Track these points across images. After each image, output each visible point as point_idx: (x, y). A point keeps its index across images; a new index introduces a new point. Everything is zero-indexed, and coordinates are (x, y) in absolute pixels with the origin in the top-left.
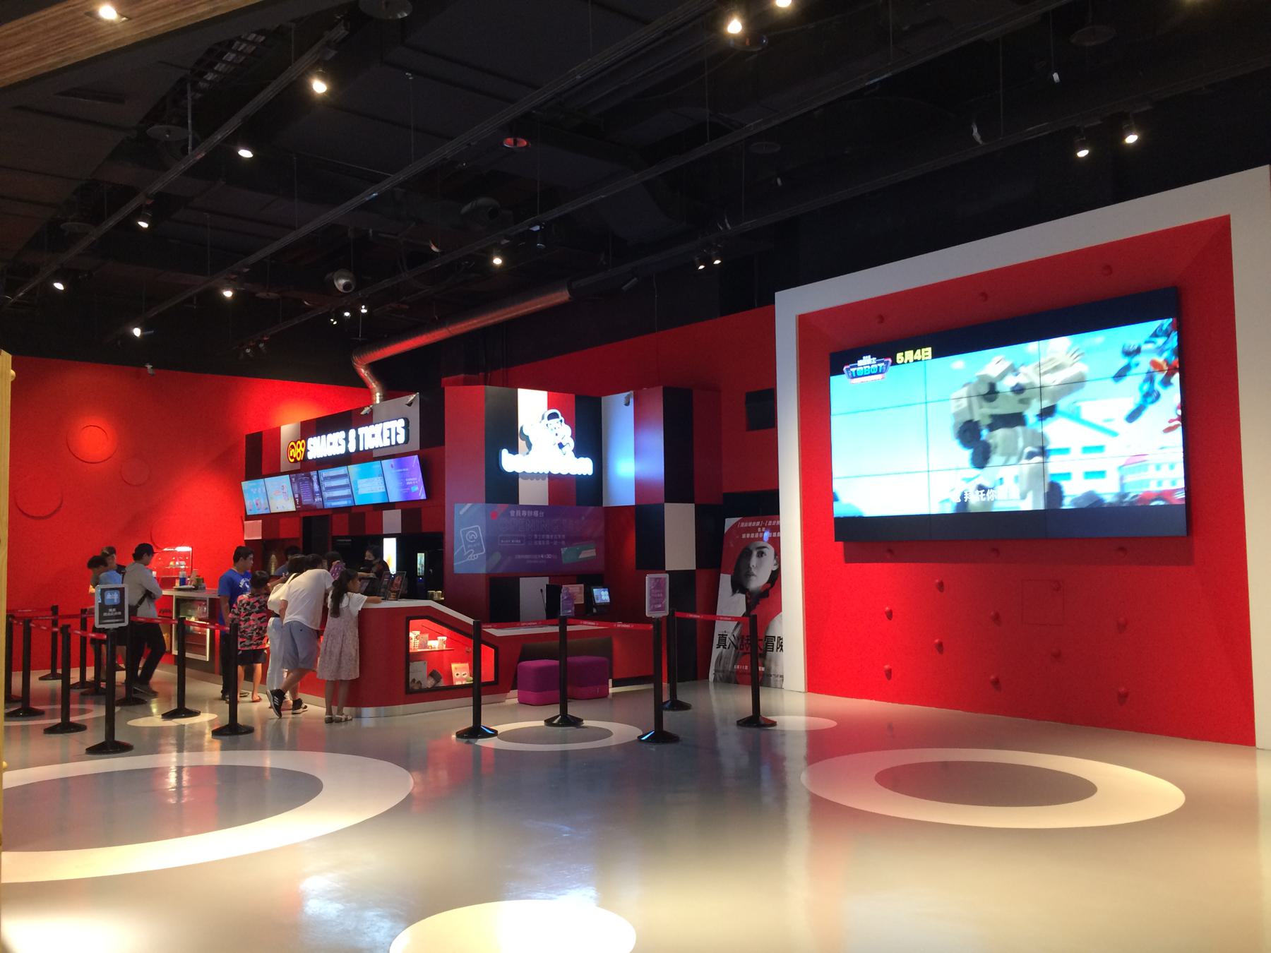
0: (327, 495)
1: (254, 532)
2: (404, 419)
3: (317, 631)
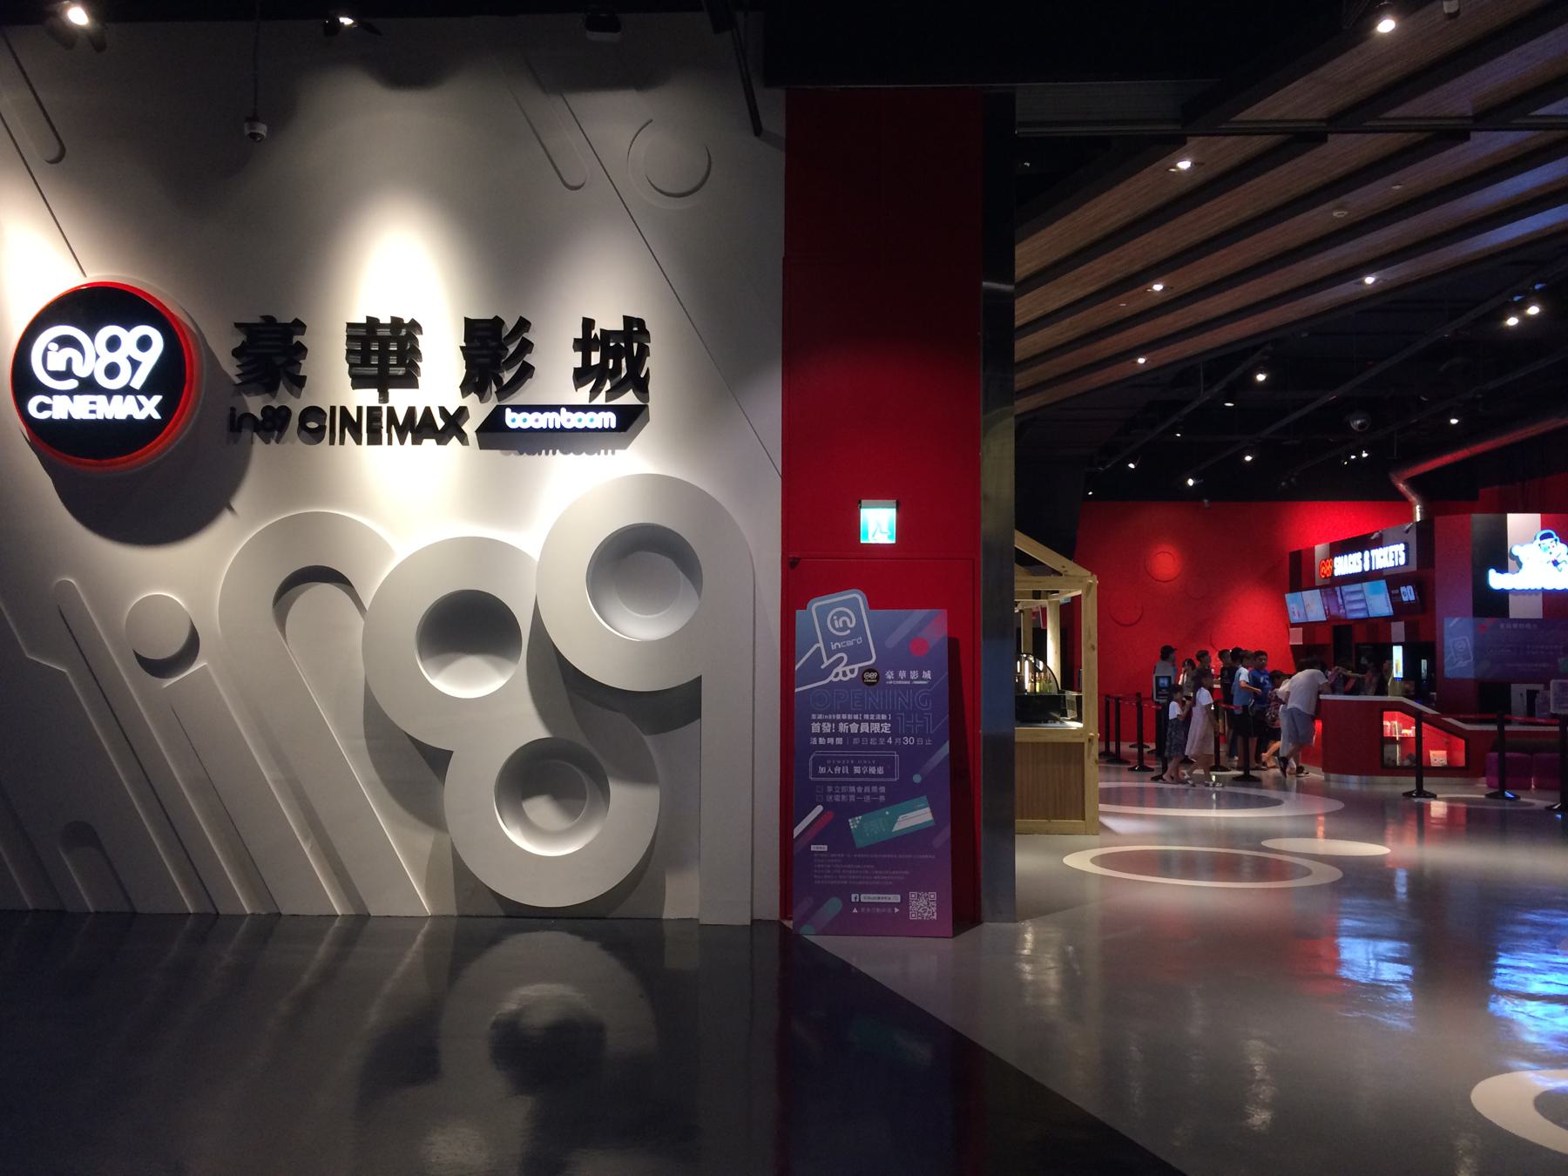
0: (1349, 607)
1: (1296, 638)
2: (1405, 544)
3: (1312, 716)
